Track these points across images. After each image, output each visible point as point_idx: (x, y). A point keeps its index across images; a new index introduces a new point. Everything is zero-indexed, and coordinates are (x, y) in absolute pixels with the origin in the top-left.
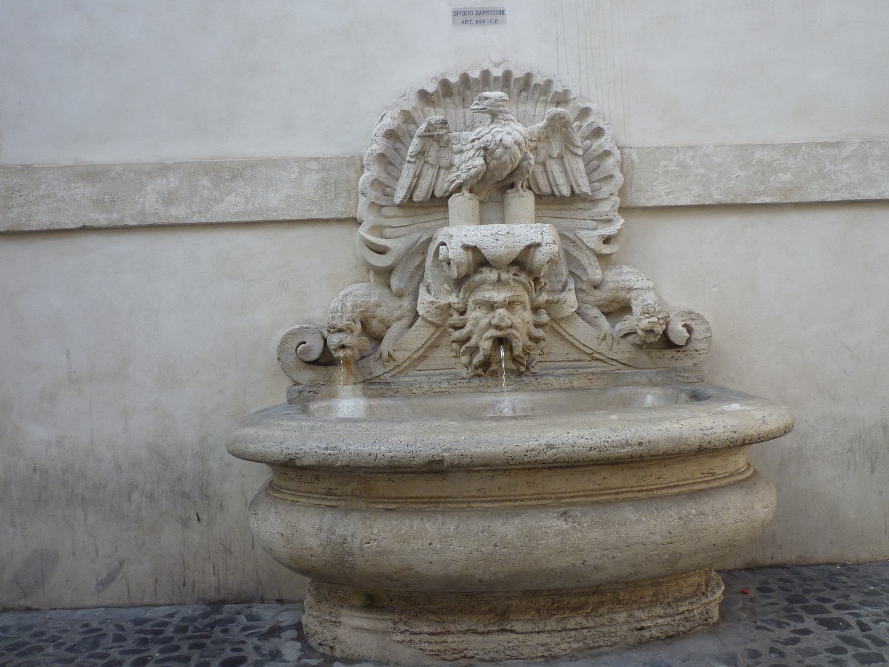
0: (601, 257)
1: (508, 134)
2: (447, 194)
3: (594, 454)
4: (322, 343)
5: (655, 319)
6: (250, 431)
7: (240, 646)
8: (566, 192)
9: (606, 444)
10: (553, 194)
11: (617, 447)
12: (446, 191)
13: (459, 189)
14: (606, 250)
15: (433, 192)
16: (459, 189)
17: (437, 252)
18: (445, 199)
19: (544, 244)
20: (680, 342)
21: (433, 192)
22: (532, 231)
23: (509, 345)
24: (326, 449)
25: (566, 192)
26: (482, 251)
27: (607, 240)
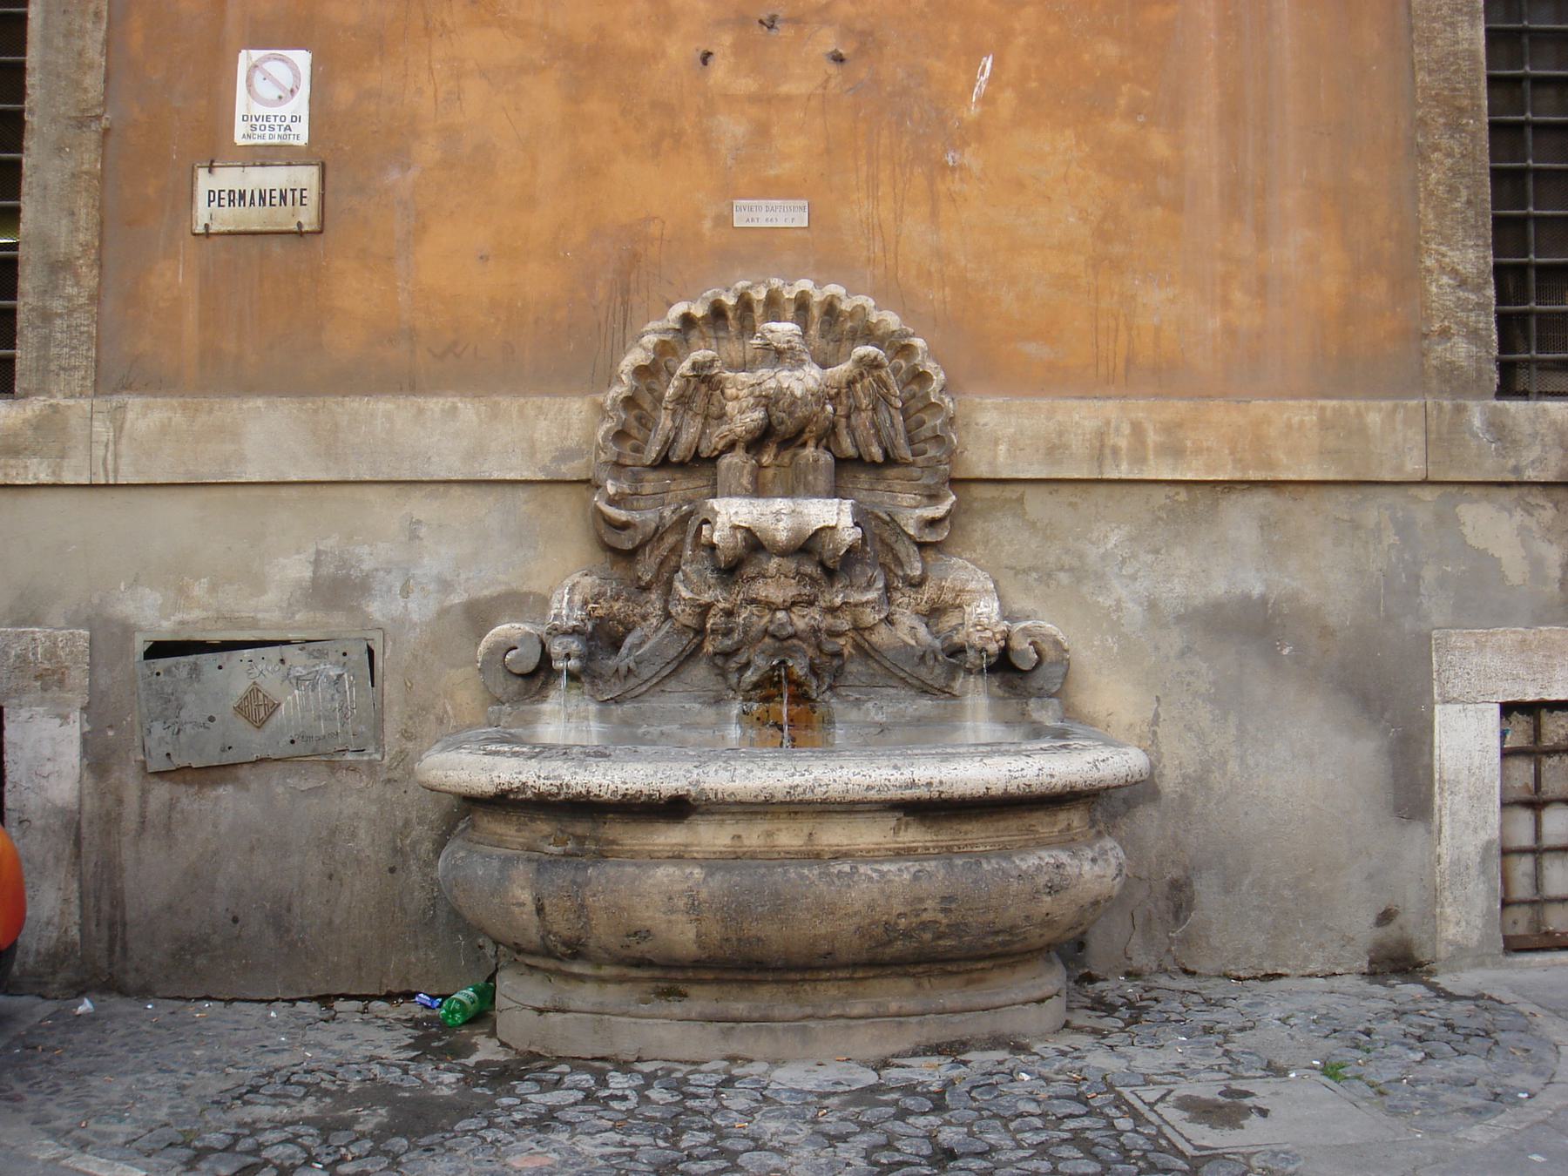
0: (922, 546)
1: (799, 379)
2: (716, 453)
3: (873, 795)
4: (539, 648)
5: (989, 634)
6: (132, 1009)
7: (816, 312)
8: (876, 453)
9: (887, 782)
10: (860, 456)
11: (901, 787)
12: (715, 449)
13: (731, 447)
14: (929, 537)
15: (697, 448)
16: (731, 447)
17: (699, 530)
18: (713, 460)
19: (840, 527)
20: (1026, 667)
21: (697, 448)
22: (825, 510)
23: (1414, 1064)
24: (546, 778)
25: (876, 453)
26: (758, 534)
27: (933, 523)
